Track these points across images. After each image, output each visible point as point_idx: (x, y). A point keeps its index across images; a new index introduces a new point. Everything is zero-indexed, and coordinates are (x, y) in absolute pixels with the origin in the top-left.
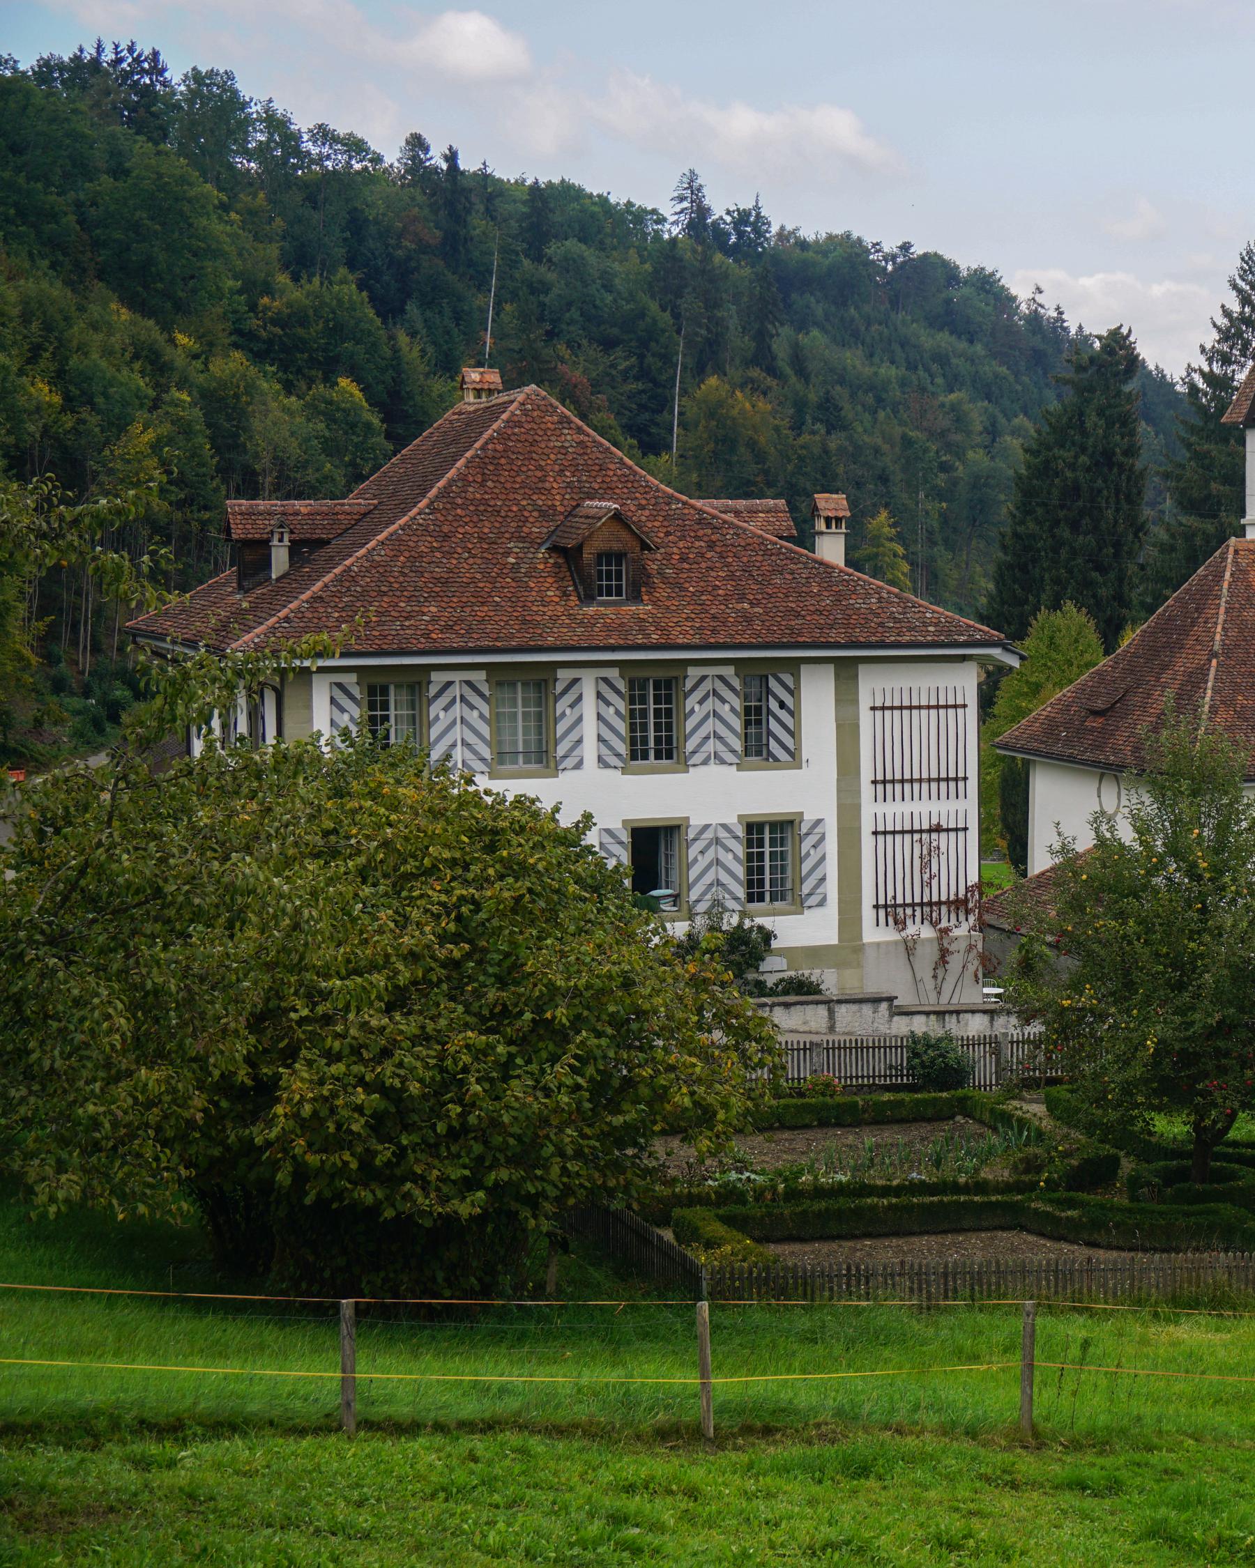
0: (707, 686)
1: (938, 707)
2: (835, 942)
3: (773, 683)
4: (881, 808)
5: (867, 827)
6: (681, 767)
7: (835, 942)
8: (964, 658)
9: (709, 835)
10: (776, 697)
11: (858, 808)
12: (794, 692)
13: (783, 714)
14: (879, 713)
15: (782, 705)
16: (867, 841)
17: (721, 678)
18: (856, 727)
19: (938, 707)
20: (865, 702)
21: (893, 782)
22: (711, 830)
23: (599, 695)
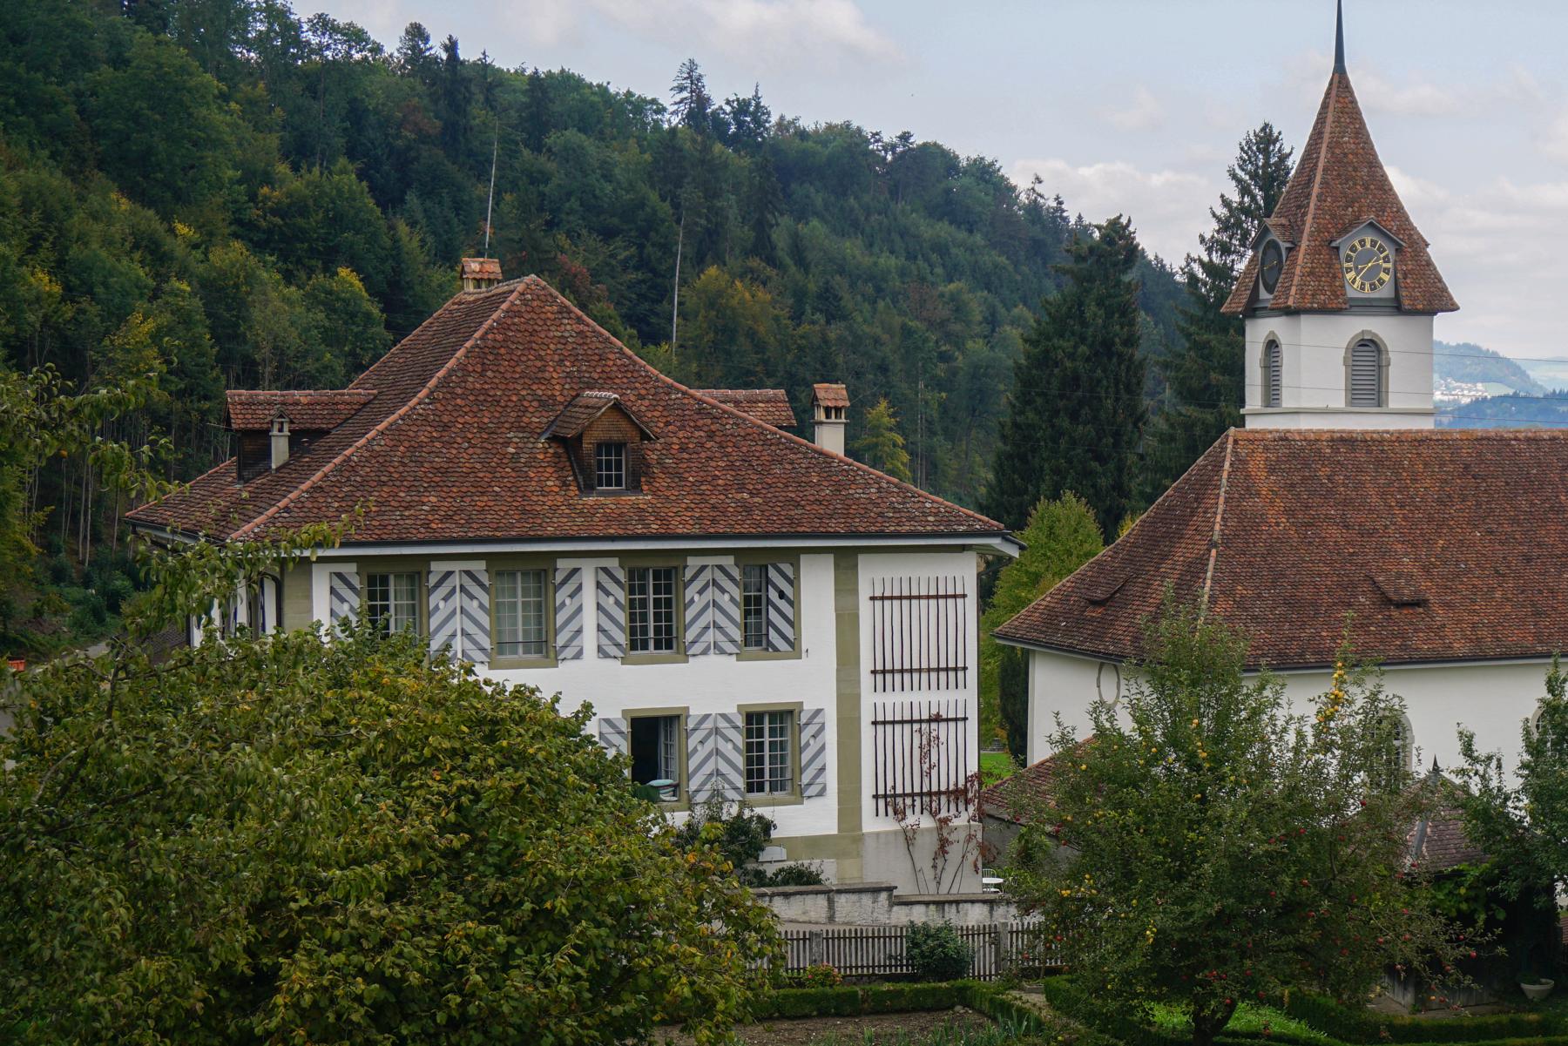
1: (937, 597)
3: (772, 573)
8: (963, 548)
9: (708, 724)
10: (776, 587)
12: (793, 582)
13: (782, 604)
15: (782, 595)
16: (867, 731)
19: (937, 597)
20: (864, 592)
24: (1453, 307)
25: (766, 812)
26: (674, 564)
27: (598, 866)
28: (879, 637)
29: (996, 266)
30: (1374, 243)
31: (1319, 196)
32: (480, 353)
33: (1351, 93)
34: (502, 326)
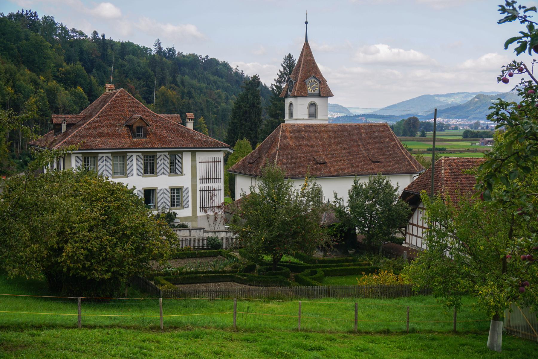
3: (177, 157)
4: (201, 185)
8: (220, 151)
9: (162, 191)
12: (182, 159)
13: (179, 164)
15: (179, 161)
16: (198, 193)
18: (196, 166)
24: (332, 96)
25: (175, 211)
28: (201, 171)
32: (110, 106)
34: (115, 100)
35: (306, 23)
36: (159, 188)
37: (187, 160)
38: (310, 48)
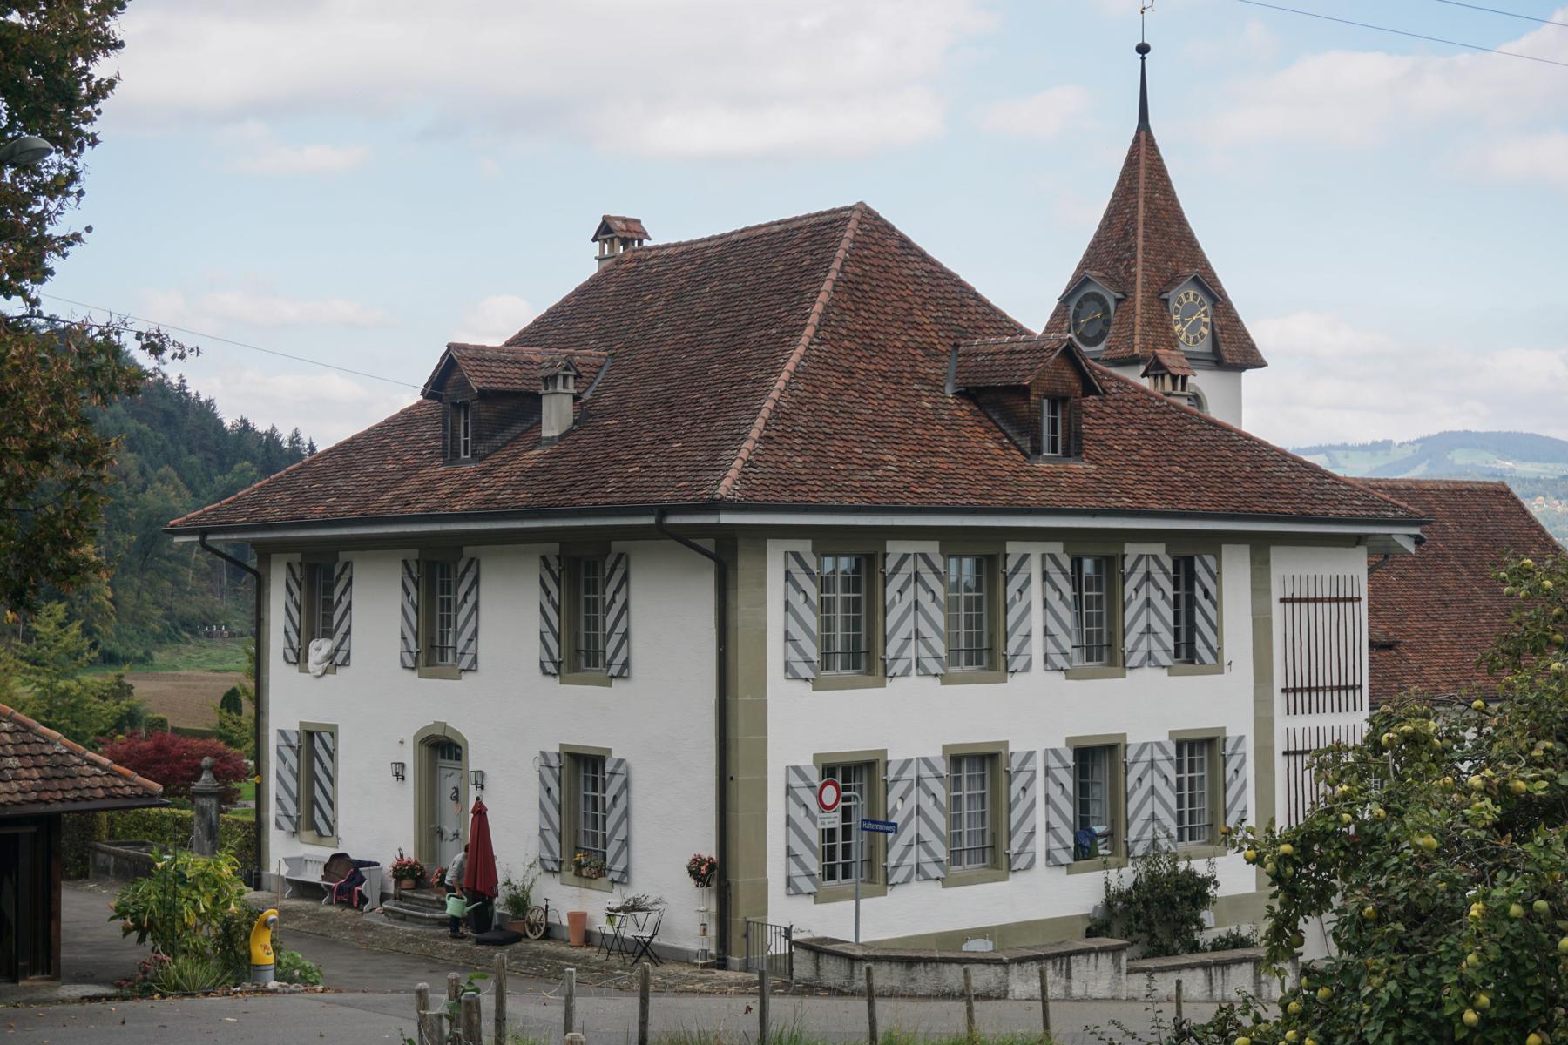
0: (908, 568)
1: (1337, 600)
2: (1253, 890)
3: (1198, 566)
4: (1302, 722)
5: (1280, 747)
6: (1118, 669)
7: (1253, 890)
8: (1358, 540)
9: (910, 774)
10: (1202, 585)
11: (1270, 722)
12: (1216, 578)
13: (1206, 604)
14: (1289, 606)
15: (1207, 594)
16: (1280, 763)
17: (924, 556)
18: (1269, 621)
19: (1337, 600)
20: (1276, 594)
21: (1332, 688)
22: (914, 764)
23: (788, 575)
24: (1261, 364)
25: (1200, 867)
26: (1112, 551)
27: (1284, 939)
28: (1292, 644)
29: (139, 432)
30: (1196, 297)
31: (1145, 248)
32: (847, 286)
33: (1156, 150)
34: (854, 258)
35: (1143, 49)
36: (1134, 739)
37: (1234, 579)
38: (1160, 160)
